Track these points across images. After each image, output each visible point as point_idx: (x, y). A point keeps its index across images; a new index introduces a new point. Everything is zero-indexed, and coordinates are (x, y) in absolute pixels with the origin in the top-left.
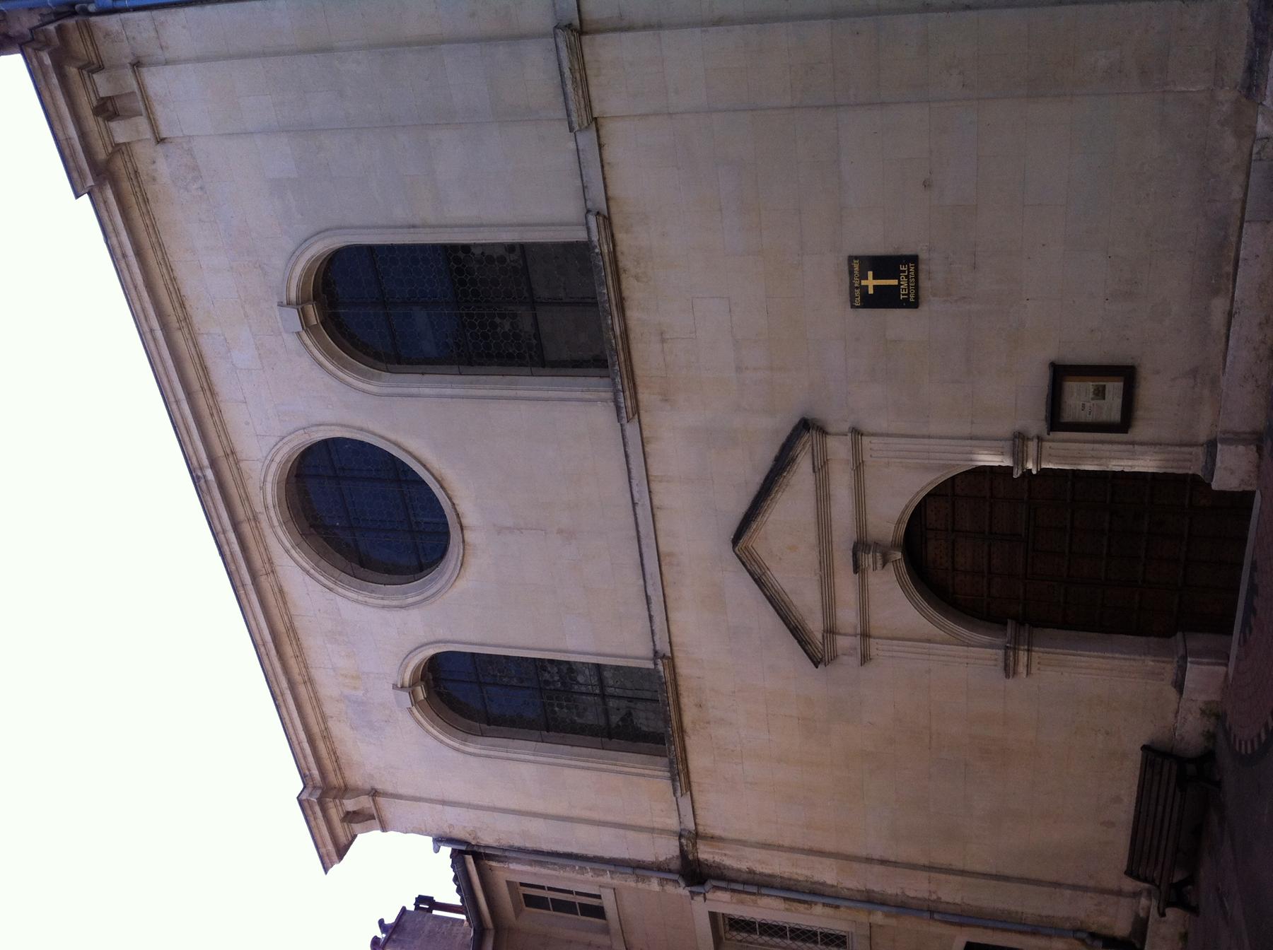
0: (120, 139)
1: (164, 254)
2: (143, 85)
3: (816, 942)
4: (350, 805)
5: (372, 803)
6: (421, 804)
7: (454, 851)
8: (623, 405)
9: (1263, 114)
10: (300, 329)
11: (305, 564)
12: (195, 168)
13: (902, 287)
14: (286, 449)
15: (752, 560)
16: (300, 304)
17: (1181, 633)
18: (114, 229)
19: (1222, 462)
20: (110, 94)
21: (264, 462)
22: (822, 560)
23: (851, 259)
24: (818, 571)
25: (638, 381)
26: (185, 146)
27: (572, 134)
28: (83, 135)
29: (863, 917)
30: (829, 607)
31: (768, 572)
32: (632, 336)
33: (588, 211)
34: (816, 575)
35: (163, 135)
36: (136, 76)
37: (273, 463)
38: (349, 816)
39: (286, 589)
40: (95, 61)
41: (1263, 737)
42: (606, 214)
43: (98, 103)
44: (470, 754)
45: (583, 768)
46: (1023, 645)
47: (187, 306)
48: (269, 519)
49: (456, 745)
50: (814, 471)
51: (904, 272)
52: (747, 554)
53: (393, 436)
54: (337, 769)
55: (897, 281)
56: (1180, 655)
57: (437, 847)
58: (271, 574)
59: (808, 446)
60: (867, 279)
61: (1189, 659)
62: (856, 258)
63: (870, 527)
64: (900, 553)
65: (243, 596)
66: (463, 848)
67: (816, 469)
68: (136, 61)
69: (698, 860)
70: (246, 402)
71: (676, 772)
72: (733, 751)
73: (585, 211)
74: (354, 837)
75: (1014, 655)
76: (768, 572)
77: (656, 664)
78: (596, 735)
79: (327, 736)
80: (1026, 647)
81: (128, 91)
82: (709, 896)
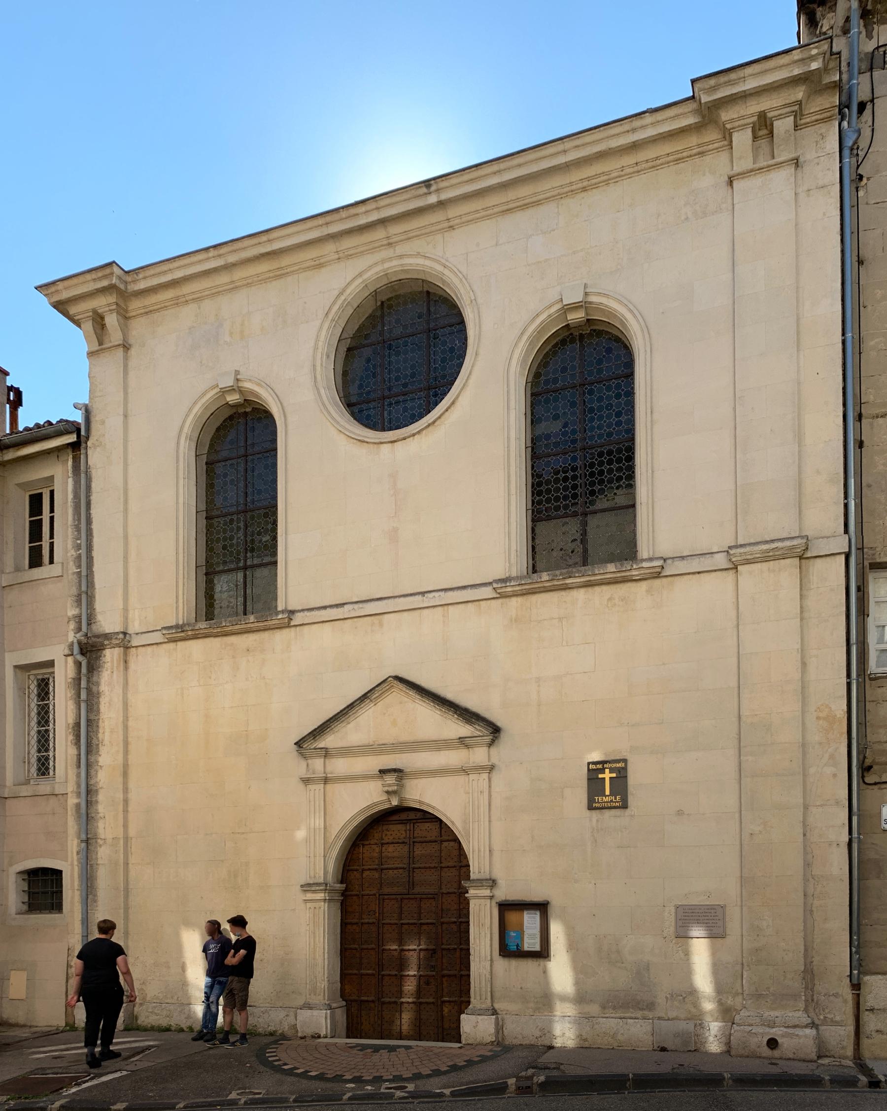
0: (736, 137)
1: (630, 175)
4: (111, 320)
5: (117, 343)
9: (726, 1025)
11: (348, 291)
14: (455, 281)
15: (382, 691)
17: (345, 1004)
19: (481, 1020)
21: (443, 258)
23: (625, 761)
24: (377, 743)
25: (525, 597)
26: (724, 205)
28: (744, 96)
29: (71, 787)
30: (347, 752)
31: (373, 704)
32: (563, 593)
34: (374, 742)
35: (735, 183)
37: (443, 268)
38: (99, 319)
39: (323, 270)
40: (803, 121)
42: (661, 575)
44: (178, 443)
46: (328, 896)
49: (186, 430)
50: (460, 738)
51: (616, 799)
52: (387, 687)
53: (471, 381)
54: (147, 310)
57: (80, 406)
58: (337, 256)
61: (329, 1011)
62: (626, 765)
63: (416, 781)
64: (396, 804)
66: (83, 433)
67: (462, 740)
70: (497, 245)
71: (185, 629)
73: (664, 558)
75: (321, 890)
76: (373, 704)
79: (178, 302)
80: (327, 898)
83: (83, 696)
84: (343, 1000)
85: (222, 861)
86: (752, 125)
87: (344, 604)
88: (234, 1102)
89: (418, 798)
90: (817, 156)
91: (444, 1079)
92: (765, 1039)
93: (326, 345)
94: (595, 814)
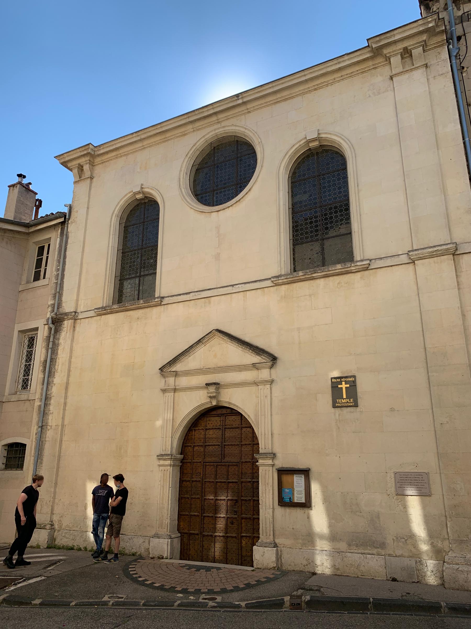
1: (339, 81)
3: (24, 376)
6: (87, 198)
7: (66, 213)
8: (280, 278)
9: (439, 563)
11: (198, 144)
12: (379, 93)
14: (251, 134)
16: (318, 139)
22: (211, 369)
23: (354, 377)
24: (205, 367)
25: (290, 285)
28: (395, 42)
29: (38, 396)
30: (188, 373)
31: (204, 346)
32: (312, 282)
33: (370, 260)
34: (203, 367)
35: (394, 79)
40: (427, 48)
41: (140, 579)
42: (369, 268)
43: (409, 49)
44: (111, 218)
45: (106, 268)
46: (173, 463)
47: (315, 92)
48: (219, 128)
49: (115, 212)
50: (253, 364)
51: (350, 401)
52: (212, 336)
53: (259, 179)
54: (102, 162)
55: (345, 398)
57: (68, 205)
58: (193, 130)
59: (264, 361)
61: (169, 540)
62: (355, 379)
63: (226, 390)
64: (215, 404)
65: (183, 117)
66: (67, 217)
72: (117, 334)
75: (168, 459)
78: (121, 274)
79: (117, 157)
80: (172, 464)
82: (46, 327)
83: (50, 346)
84: (179, 533)
85: (114, 439)
87: (190, 293)
88: (105, 603)
94: (338, 411)
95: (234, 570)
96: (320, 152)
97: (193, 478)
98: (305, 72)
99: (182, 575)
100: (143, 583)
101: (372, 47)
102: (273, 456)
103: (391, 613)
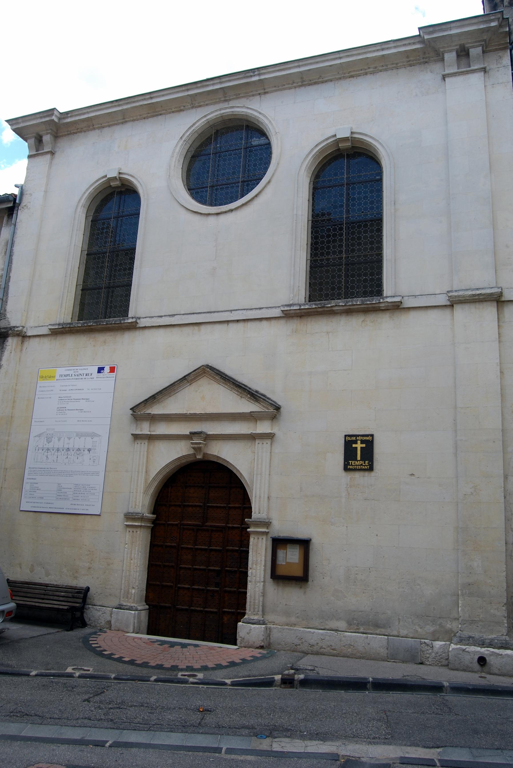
0: (447, 56)
2: (474, 72)
7: (16, 196)
10: (338, 137)
13: (356, 462)
15: (197, 375)
18: (398, 46)
20: (470, 54)
23: (372, 436)
27: (446, 292)
31: (189, 384)
35: (446, 79)
36: (479, 69)
40: (488, 49)
48: (226, 108)
51: (365, 463)
56: (138, 607)
60: (361, 444)
62: (373, 438)
65: (181, 89)
66: (17, 201)
68: (487, 71)
69: (8, 337)
73: (402, 296)
74: (26, 140)
76: (189, 384)
77: (132, 318)
81: (471, 64)
84: (147, 605)
86: (456, 50)
87: (175, 315)
88: (70, 676)
89: (216, 454)
90: (497, 67)
91: (225, 672)
92: (477, 657)
93: (179, 154)
95: (214, 648)
96: (351, 154)
97: (167, 543)
98: (341, 54)
99: (154, 651)
100: (109, 657)
101: (424, 38)
102: (267, 524)
103: (391, 692)
